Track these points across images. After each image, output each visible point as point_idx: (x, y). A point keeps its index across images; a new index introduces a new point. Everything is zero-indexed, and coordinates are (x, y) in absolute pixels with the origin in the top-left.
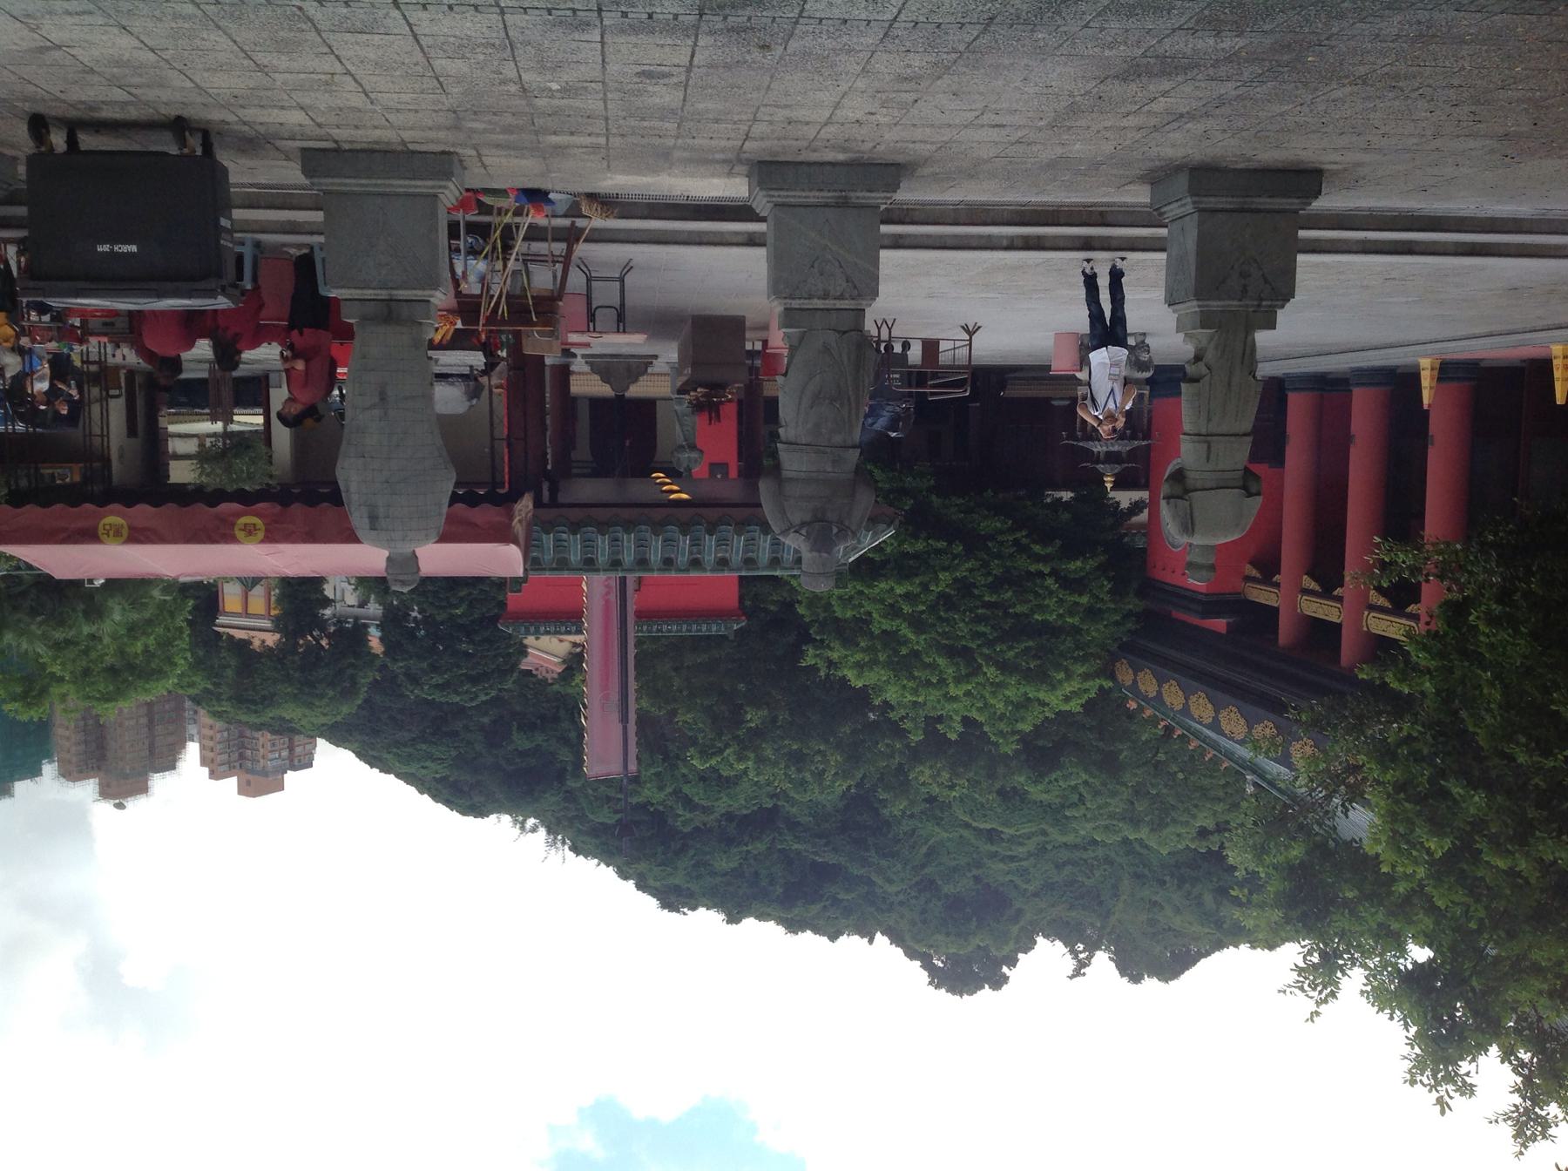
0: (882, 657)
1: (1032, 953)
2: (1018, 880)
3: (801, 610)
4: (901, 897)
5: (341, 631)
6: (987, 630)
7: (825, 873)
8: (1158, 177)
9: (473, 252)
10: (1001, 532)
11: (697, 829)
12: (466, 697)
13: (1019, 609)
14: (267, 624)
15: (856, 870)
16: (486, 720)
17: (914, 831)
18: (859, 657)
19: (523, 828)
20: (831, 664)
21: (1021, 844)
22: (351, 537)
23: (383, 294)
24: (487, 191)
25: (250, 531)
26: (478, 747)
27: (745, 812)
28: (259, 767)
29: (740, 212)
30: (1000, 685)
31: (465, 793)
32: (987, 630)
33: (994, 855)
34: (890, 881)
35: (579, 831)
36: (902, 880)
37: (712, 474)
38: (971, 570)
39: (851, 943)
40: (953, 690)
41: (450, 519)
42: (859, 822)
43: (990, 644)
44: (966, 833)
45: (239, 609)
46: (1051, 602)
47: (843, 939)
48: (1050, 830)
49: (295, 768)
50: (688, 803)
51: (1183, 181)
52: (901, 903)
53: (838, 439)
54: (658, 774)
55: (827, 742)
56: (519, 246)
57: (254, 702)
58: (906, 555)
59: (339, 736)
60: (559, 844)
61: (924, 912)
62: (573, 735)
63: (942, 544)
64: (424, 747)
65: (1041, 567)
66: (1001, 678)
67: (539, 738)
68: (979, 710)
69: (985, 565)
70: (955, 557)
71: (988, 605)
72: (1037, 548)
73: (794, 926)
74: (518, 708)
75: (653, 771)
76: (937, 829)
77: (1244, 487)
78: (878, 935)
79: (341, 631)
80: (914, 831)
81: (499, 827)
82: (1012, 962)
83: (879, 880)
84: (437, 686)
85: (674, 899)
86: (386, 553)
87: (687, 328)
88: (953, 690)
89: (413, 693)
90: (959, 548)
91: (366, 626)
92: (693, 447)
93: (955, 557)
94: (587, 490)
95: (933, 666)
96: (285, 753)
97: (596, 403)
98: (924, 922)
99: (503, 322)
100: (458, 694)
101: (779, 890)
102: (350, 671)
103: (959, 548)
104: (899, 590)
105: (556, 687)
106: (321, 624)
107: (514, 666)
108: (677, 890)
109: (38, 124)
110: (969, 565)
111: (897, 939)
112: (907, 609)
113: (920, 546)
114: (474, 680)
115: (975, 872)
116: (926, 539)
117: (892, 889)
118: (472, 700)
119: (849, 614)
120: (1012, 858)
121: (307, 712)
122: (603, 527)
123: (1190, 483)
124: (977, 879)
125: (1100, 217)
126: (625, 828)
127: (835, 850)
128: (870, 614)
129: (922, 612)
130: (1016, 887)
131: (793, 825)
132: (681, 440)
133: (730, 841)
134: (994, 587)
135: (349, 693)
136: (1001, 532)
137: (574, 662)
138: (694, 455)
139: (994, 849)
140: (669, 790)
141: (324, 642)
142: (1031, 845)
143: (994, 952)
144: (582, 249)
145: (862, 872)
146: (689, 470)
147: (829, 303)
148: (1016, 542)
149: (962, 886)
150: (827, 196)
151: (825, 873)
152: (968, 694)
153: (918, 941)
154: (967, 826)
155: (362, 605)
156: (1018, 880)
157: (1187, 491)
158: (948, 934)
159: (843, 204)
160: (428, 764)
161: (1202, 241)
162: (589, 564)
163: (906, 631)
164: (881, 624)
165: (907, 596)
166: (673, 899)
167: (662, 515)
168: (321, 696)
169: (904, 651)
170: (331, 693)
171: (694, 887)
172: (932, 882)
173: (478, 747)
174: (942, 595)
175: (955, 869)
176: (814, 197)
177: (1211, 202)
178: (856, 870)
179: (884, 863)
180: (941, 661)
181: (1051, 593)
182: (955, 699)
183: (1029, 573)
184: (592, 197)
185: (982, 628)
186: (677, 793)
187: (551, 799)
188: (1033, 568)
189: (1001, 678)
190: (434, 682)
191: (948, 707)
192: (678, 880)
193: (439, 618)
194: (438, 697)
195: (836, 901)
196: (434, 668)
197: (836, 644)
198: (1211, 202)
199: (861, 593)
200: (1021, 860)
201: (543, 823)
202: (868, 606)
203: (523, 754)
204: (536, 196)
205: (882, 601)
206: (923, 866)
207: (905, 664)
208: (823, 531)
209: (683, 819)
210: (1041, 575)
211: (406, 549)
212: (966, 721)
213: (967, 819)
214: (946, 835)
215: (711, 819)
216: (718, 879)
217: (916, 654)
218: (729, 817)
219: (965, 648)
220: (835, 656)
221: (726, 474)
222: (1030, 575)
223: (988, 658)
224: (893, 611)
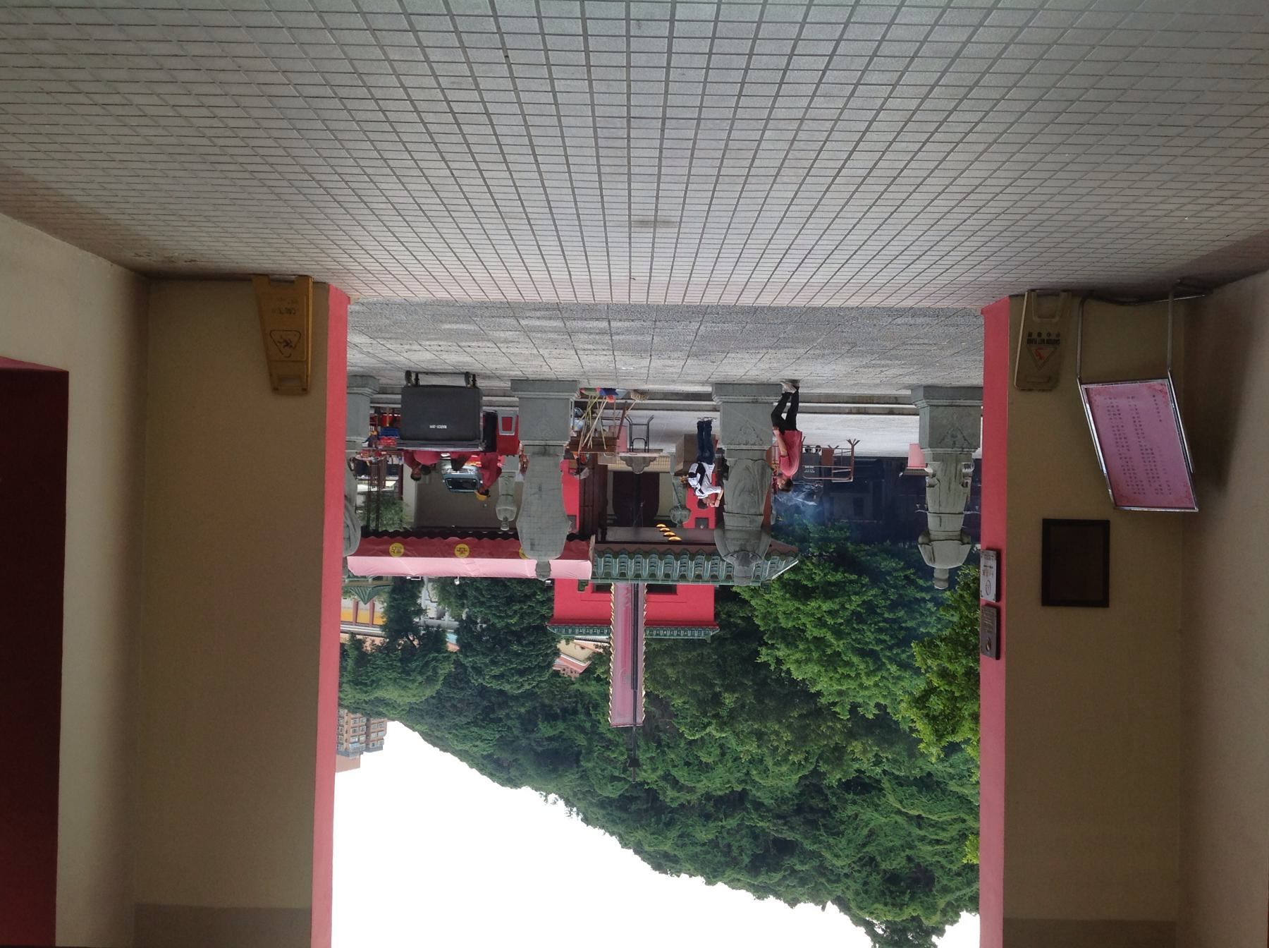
0: (815, 655)
1: (956, 925)
2: (943, 861)
3: (757, 621)
4: (846, 871)
5: (429, 633)
6: (887, 638)
7: (785, 847)
8: (914, 388)
9: (577, 416)
10: (896, 570)
11: (682, 805)
12: (515, 686)
13: (910, 624)
14: (378, 631)
15: (809, 846)
16: (523, 710)
17: (856, 815)
18: (798, 656)
19: (546, 800)
20: (779, 662)
21: (944, 830)
22: (516, 555)
23: (543, 443)
24: (586, 389)
25: (462, 551)
26: (516, 732)
27: (720, 793)
28: (342, 749)
29: (707, 397)
30: (899, 678)
31: (503, 768)
32: (887, 638)
33: (922, 839)
34: (837, 856)
35: (591, 803)
36: (847, 856)
37: (697, 526)
38: (875, 596)
39: (807, 909)
40: (867, 683)
41: (567, 548)
42: (813, 807)
43: (890, 648)
44: (899, 819)
45: (351, 619)
46: (932, 620)
47: (801, 906)
48: (967, 818)
49: (368, 750)
50: (675, 783)
51: (921, 393)
52: (846, 876)
53: (752, 511)
54: (652, 759)
55: (780, 722)
56: (600, 412)
57: (366, 685)
58: (830, 583)
59: (412, 717)
60: (574, 815)
61: (865, 884)
62: (588, 725)
63: (854, 577)
64: (475, 729)
65: (923, 595)
66: (899, 673)
67: (561, 726)
68: (884, 697)
69: (885, 592)
70: (863, 586)
71: (885, 620)
72: (921, 582)
73: (761, 891)
74: (547, 702)
75: (648, 755)
76: (876, 815)
77: (961, 540)
78: (829, 903)
79: (429, 633)
80: (856, 815)
81: (527, 794)
82: (940, 932)
83: (828, 855)
84: (495, 677)
85: (663, 862)
86: (535, 562)
87: (682, 440)
88: (868, 682)
89: (476, 681)
90: (866, 580)
91: (444, 631)
92: (684, 507)
93: (863, 586)
94: (615, 534)
95: (848, 664)
96: (363, 738)
97: (618, 475)
98: (866, 892)
99: (590, 450)
100: (508, 682)
101: (746, 860)
102: (434, 663)
103: (866, 580)
104: (825, 607)
105: (576, 686)
106: (415, 629)
107: (550, 664)
108: (666, 856)
109: (408, 374)
110: (873, 592)
111: (844, 906)
112: (830, 621)
113: (839, 576)
114: (521, 673)
115: (908, 852)
116: (843, 573)
117: (839, 863)
118: (519, 688)
119: (790, 624)
120: (938, 842)
121: (403, 693)
122: (631, 555)
123: (932, 537)
124: (909, 859)
125: (896, 400)
126: (623, 803)
127: (792, 828)
128: (804, 624)
129: (841, 624)
130: (942, 867)
131: (758, 805)
132: (676, 503)
133: (707, 817)
134: (893, 607)
135: (430, 680)
136: (896, 570)
137: (600, 659)
138: (685, 512)
139: (922, 833)
140: (660, 773)
141: (416, 643)
142: (953, 831)
143: (926, 923)
144: (629, 412)
145: (815, 847)
146: (681, 522)
147: (748, 447)
148: (906, 577)
149: (896, 863)
150: (747, 398)
151: (785, 847)
152: (876, 685)
153: (861, 909)
154: (899, 812)
155: (440, 617)
156: (943, 861)
157: (931, 541)
158: (886, 904)
159: (756, 402)
160: (478, 743)
161: (931, 418)
162: (623, 576)
163: (830, 637)
164: (813, 632)
165: (831, 613)
166: (662, 861)
167: (666, 549)
168: (414, 681)
169: (829, 651)
170: (420, 679)
171: (680, 854)
172: (872, 859)
173: (516, 732)
174: (854, 612)
175: (892, 849)
176: (742, 399)
177: (935, 402)
178: (809, 846)
179: (831, 841)
180: (855, 660)
181: (932, 613)
182: (866, 688)
183: (916, 599)
184: (636, 391)
185: (883, 637)
186: (666, 777)
187: (571, 777)
188: (918, 595)
189: (899, 673)
190: (493, 673)
191: (862, 693)
192: (667, 847)
193: (499, 625)
194: (495, 685)
195: (793, 872)
196: (493, 663)
197: (782, 646)
198: (935, 402)
199: (798, 609)
200: (945, 843)
201: (561, 797)
202: (804, 619)
203: (550, 739)
204: (610, 392)
205: (813, 615)
206: (864, 845)
207: (832, 661)
208: (745, 555)
209: (670, 796)
210: (924, 600)
211: (545, 559)
212: (878, 705)
213: (899, 806)
214: (884, 820)
215: (693, 798)
216: (699, 849)
217: (838, 654)
218: (708, 797)
219: (872, 651)
220: (780, 654)
221: (707, 527)
222: (918, 601)
223: (891, 660)
224: (821, 623)
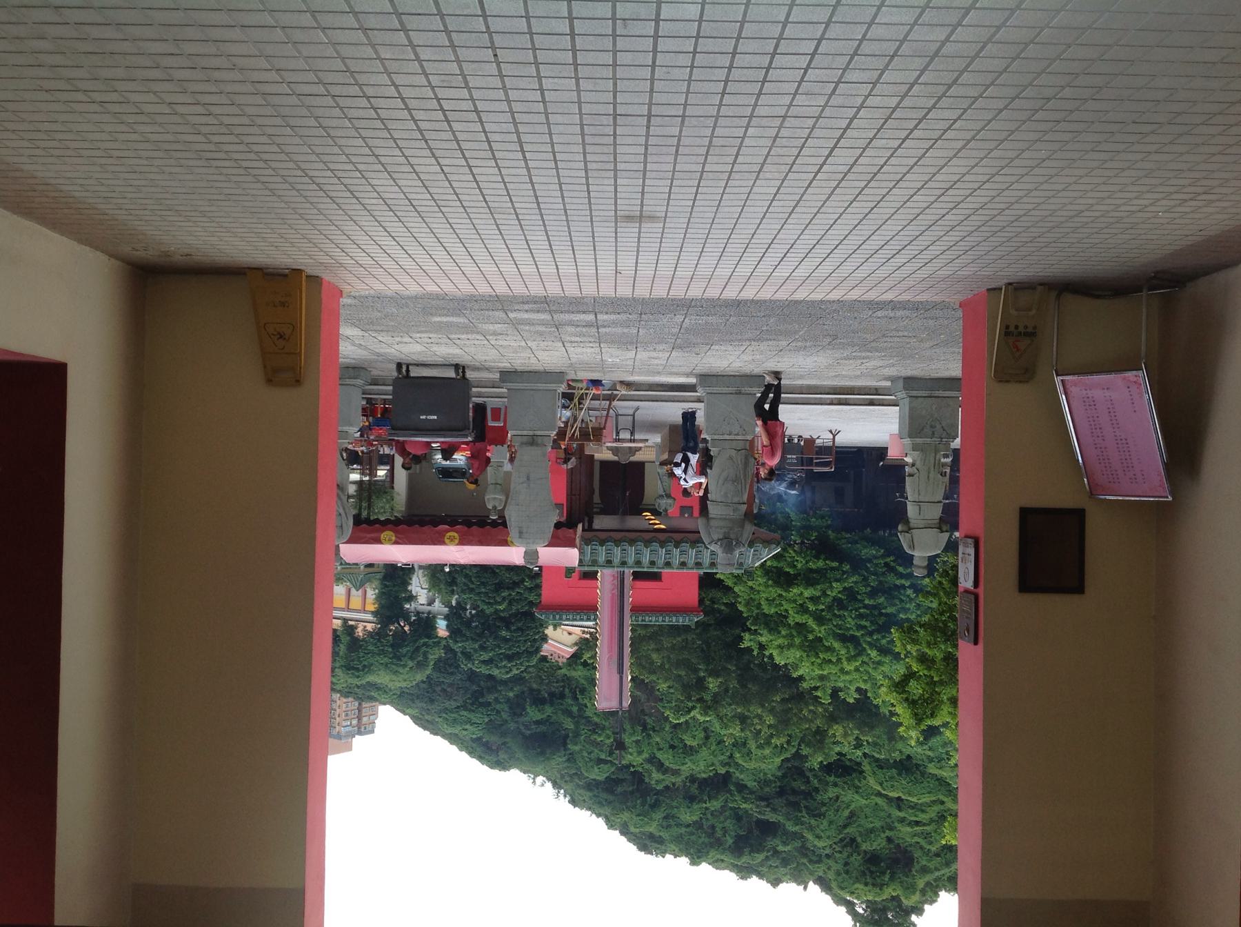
0: (797, 641)
1: (935, 905)
2: (923, 842)
3: (741, 608)
4: (828, 851)
5: (419, 619)
6: (867, 624)
7: (768, 829)
8: (893, 379)
9: (565, 407)
10: (876, 558)
11: (667, 787)
12: (503, 671)
13: (890, 610)
14: (369, 617)
15: (791, 827)
16: (511, 694)
17: (838, 797)
18: (780, 641)
19: (534, 782)
20: (762, 647)
21: (923, 811)
22: (504, 543)
23: (531, 433)
24: (573, 381)
25: (452, 539)
26: (504, 715)
27: (704, 776)
28: (335, 732)
29: (692, 388)
30: (879, 663)
31: (492, 751)
32: (867, 624)
33: (902, 820)
34: (819, 837)
35: (578, 786)
36: (828, 837)
37: (682, 514)
38: (856, 583)
39: (789, 889)
40: (848, 667)
41: (554, 536)
42: (795, 789)
43: (871, 634)
44: (879, 800)
45: (343, 605)
46: (912, 606)
47: (783, 886)
48: (945, 799)
49: (360, 733)
50: (660, 766)
51: (901, 384)
52: (828, 856)
53: (736, 500)
54: (637, 742)
55: (763, 706)
56: (587, 403)
57: (358, 670)
58: (811, 570)
59: (403, 701)
60: (562, 797)
61: (846, 864)
62: (575, 709)
63: (835, 564)
64: (465, 713)
65: (903, 581)
66: (879, 658)
67: (549, 710)
68: (865, 681)
69: (865, 579)
70: (844, 573)
71: (866, 607)
72: (901, 569)
73: (744, 872)
74: (535, 686)
75: (634, 739)
76: (857, 797)
77: (940, 528)
78: (811, 883)
79: (419, 619)
80: (838, 797)
81: (515, 776)
82: (919, 911)
83: (809, 836)
84: (484, 662)
85: (649, 843)
86: (524, 549)
87: (667, 430)
88: (849, 667)
89: (466, 666)
90: (847, 567)
91: (434, 617)
92: (668, 496)
93: (844, 573)
94: (601, 522)
95: (830, 649)
96: (355, 722)
97: (605, 464)
98: (847, 872)
99: (577, 440)
100: (497, 667)
101: (730, 841)
102: (424, 648)
103: (847, 567)
104: (807, 593)
105: (564, 671)
106: (405, 615)
107: (538, 650)
108: (651, 837)
109: (399, 365)
110: (854, 579)
111: (825, 885)
112: (812, 607)
113: (820, 564)
114: (510, 658)
115: (888, 833)
116: (825, 560)
117: (820, 844)
118: (507, 673)
119: (773, 611)
120: (917, 823)
121: (394, 678)
122: (617, 543)
123: (912, 525)
124: (889, 840)
125: (876, 391)
126: (609, 785)
127: (774, 810)
128: (786, 611)
129: (823, 610)
130: (922, 848)
131: (741, 788)
132: (661, 492)
133: (692, 799)
134: (873, 593)
135: (421, 665)
136: (876, 558)
137: (587, 644)
138: (670, 501)
139: (902, 814)
140: (645, 755)
141: (406, 628)
142: (932, 813)
143: (905, 902)
144: (615, 403)
145: (797, 828)
146: (666, 510)
147: (732, 437)
148: (886, 564)
149: (876, 844)
150: (731, 389)
151: (768, 829)
152: (857, 670)
153: (842, 889)
154: (879, 794)
155: (430, 603)
156: (923, 842)
157: (910, 529)
158: (866, 884)
159: (739, 393)
160: (467, 727)
161: (911, 409)
162: (609, 563)
163: (811, 623)
164: (795, 618)
165: (813, 599)
166: (647, 842)
167: (651, 537)
168: (404, 666)
169: (811, 637)
170: (411, 664)
171: (665, 835)
172: (853, 840)
173: (504, 715)
174: (835, 599)
175: (872, 831)
176: (725, 390)
177: (914, 393)
178: (791, 827)
179: (813, 822)
180: (836, 645)
181: (911, 600)
182: (847, 673)
183: (896, 586)
184: (622, 382)
185: (863, 623)
186: (652, 760)
187: (558, 760)
188: (898, 582)
189: (879, 658)
190: (482, 658)
191: (843, 678)
192: (652, 828)
193: (488, 612)
194: (484, 670)
195: (776, 853)
196: (483, 648)
197: (765, 632)
198: (914, 393)
199: (780, 596)
200: (924, 825)
201: (549, 779)
202: (786, 606)
203: (538, 723)
204: (596, 383)
205: (795, 601)
206: (845, 826)
207: (814, 647)
208: (729, 543)
209: (655, 778)
210: (903, 587)
211: (533, 547)
212: (858, 690)
213: (879, 788)
214: (864, 802)
215: (678, 780)
216: (683, 830)
217: (820, 640)
218: (692, 779)
219: (853, 637)
220: (763, 639)
221: (691, 515)
222: (898, 588)
223: (871, 645)
224: (803, 609)
